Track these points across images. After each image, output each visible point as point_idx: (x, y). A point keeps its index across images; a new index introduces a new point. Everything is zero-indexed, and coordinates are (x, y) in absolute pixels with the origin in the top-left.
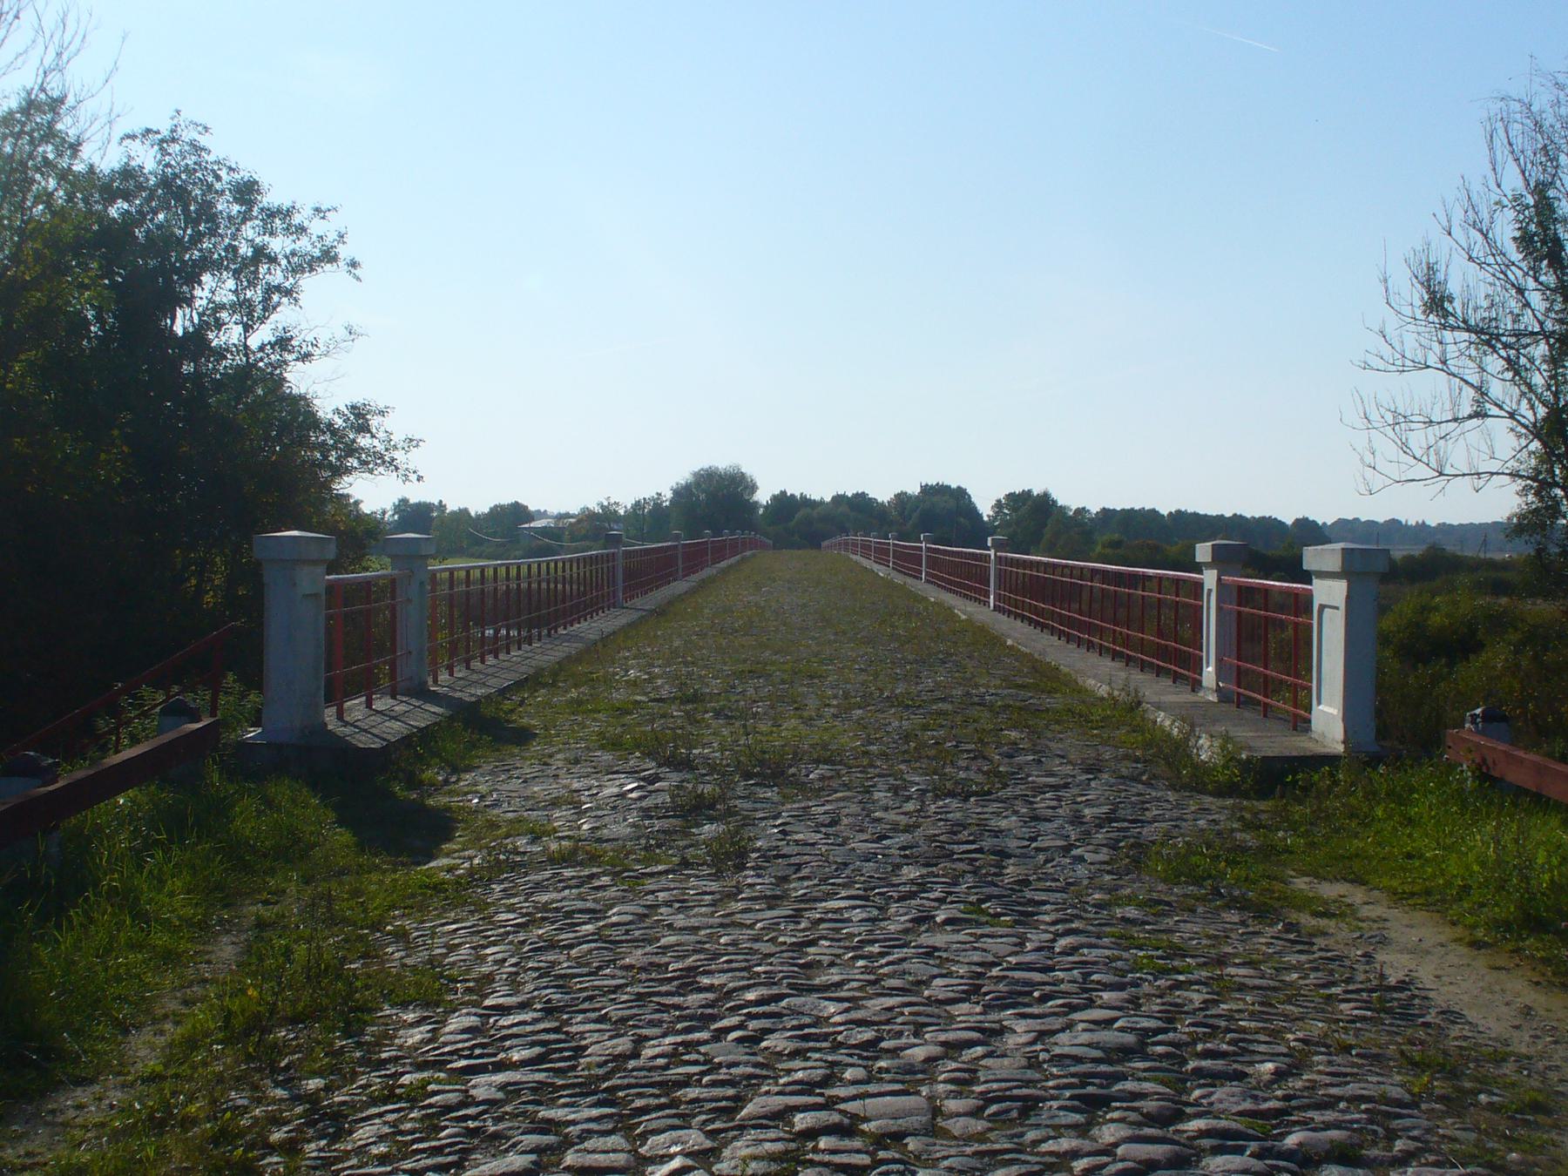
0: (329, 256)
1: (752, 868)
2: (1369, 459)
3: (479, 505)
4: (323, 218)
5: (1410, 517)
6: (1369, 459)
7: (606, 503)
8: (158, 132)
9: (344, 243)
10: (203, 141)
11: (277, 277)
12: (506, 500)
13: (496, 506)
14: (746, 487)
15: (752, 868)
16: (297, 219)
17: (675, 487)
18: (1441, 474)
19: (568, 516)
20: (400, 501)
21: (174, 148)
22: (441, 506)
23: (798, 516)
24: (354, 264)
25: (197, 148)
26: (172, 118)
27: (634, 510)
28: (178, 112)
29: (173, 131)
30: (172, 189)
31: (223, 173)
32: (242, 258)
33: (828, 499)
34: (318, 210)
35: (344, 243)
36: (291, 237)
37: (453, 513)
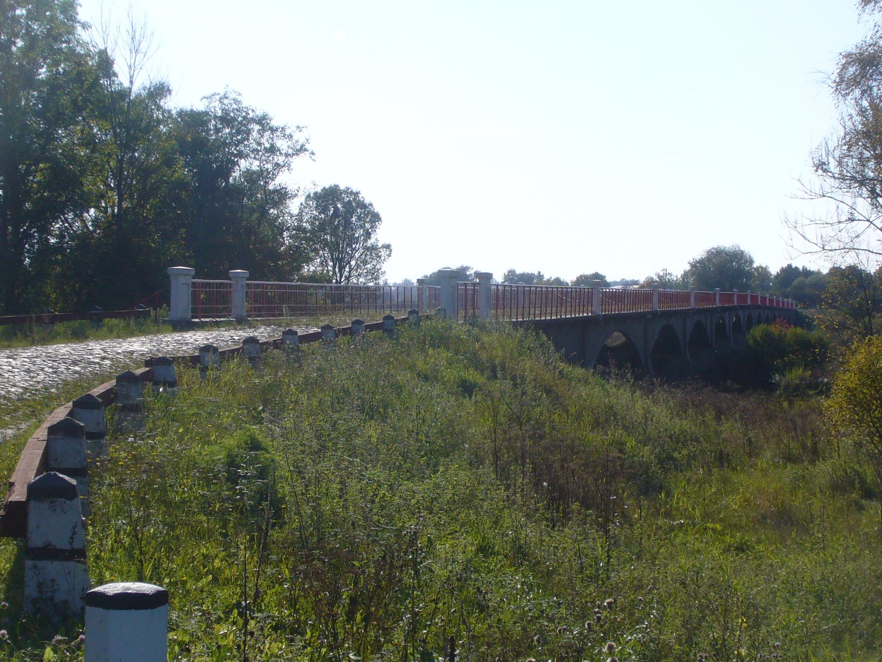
0: (302, 149)
1: (65, 218)
2: (790, 242)
3: (569, 277)
4: (301, 131)
5: (813, 268)
6: (790, 242)
7: (661, 274)
8: (219, 94)
9: (309, 143)
10: (239, 98)
11: (280, 160)
12: (589, 272)
13: (581, 276)
14: (746, 262)
15: (65, 218)
16: (288, 132)
17: (692, 261)
18: (824, 249)
19: (635, 283)
20: (509, 272)
21: (226, 101)
22: (540, 276)
23: (795, 283)
24: (313, 153)
25: (236, 101)
26: (225, 88)
27: (683, 279)
28: (227, 86)
29: (225, 95)
30: (226, 119)
31: (250, 112)
32: (231, 168)
33: (774, 270)
34: (298, 127)
35: (309, 143)
36: (286, 140)
37: (548, 280)
